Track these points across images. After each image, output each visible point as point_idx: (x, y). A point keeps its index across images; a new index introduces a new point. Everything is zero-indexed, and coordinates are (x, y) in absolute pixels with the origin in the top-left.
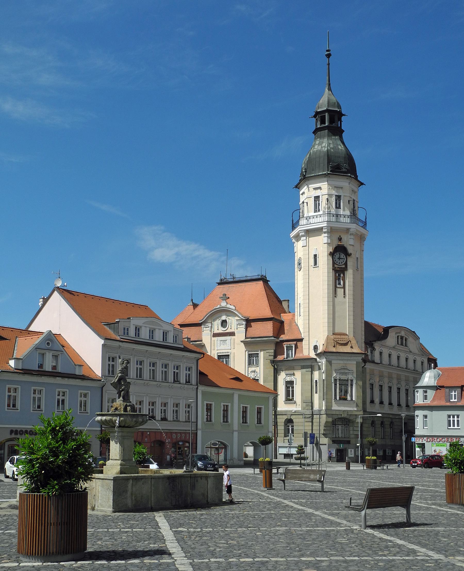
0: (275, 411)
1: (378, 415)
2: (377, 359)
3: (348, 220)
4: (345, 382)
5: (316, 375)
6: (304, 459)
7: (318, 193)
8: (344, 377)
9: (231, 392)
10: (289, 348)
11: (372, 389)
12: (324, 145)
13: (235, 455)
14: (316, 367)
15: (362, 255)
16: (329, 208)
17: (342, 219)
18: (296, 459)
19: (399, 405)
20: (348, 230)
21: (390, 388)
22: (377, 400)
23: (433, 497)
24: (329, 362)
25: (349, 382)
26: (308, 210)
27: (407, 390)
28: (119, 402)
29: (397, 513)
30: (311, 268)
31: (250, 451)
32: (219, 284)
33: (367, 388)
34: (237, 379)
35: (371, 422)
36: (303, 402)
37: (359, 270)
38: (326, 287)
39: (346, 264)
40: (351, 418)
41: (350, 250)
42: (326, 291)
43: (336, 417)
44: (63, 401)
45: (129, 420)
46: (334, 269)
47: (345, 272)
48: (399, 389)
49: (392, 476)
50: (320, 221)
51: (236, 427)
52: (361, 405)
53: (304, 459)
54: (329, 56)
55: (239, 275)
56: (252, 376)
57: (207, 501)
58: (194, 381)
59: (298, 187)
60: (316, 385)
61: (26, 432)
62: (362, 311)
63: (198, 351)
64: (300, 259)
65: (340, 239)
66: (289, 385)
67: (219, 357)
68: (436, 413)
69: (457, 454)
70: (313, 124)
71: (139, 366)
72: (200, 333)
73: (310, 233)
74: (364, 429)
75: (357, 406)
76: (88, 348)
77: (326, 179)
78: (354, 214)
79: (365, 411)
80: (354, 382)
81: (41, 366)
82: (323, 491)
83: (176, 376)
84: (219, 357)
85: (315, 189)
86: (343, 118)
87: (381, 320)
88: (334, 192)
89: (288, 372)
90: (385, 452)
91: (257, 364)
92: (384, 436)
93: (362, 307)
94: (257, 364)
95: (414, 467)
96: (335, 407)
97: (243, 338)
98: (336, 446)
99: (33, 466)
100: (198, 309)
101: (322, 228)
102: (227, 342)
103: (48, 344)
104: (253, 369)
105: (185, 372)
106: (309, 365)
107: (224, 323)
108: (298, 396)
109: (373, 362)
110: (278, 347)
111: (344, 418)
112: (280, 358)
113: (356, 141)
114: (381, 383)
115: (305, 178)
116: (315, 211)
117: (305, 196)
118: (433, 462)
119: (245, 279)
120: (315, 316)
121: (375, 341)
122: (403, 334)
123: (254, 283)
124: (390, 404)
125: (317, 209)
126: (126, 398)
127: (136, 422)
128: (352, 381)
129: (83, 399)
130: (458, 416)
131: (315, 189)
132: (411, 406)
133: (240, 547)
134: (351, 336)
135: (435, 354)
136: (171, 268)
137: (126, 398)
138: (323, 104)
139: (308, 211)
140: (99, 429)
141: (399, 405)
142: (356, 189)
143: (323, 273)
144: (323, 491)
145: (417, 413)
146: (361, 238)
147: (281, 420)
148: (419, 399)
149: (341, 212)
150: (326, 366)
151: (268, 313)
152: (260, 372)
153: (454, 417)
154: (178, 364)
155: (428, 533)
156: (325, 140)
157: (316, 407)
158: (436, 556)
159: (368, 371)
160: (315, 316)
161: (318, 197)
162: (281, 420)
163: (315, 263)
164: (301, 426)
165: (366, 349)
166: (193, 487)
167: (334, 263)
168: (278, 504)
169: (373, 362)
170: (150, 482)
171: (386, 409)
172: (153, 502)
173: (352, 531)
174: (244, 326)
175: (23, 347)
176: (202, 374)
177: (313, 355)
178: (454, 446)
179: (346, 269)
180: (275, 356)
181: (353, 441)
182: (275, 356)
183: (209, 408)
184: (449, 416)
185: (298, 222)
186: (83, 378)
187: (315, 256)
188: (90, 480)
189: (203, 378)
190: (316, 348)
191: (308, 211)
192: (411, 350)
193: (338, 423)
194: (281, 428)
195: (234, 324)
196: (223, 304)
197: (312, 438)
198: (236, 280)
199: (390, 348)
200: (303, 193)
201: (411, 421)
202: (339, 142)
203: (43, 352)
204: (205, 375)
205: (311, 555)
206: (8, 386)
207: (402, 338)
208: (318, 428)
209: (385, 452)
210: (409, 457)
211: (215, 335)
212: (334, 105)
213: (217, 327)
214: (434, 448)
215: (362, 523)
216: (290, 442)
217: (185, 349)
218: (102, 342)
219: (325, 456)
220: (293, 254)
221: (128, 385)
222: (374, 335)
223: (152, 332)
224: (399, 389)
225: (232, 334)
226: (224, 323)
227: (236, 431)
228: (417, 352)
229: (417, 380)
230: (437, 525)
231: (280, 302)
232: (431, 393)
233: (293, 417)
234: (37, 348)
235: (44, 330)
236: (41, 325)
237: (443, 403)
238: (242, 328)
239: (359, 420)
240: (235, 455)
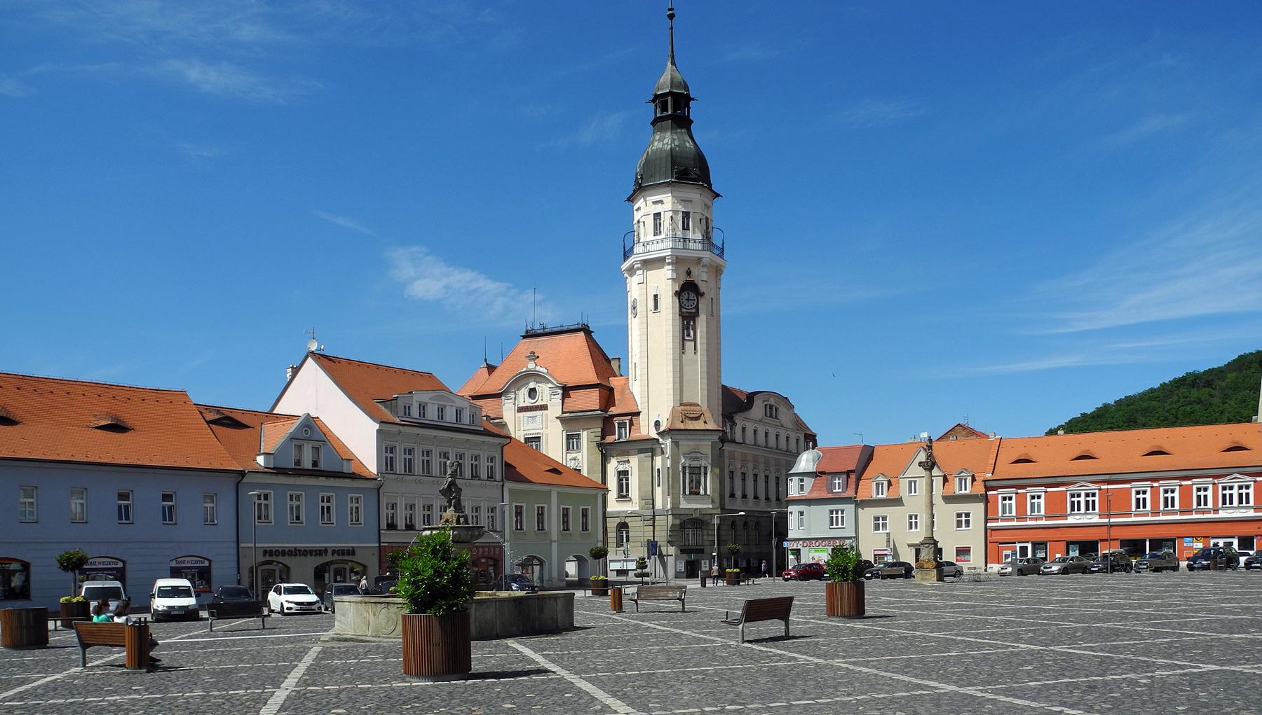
0: (604, 513)
2: (738, 438)
3: (699, 246)
4: (697, 471)
5: (658, 461)
6: (647, 575)
7: (658, 208)
9: (547, 488)
10: (622, 425)
11: (732, 478)
13: (555, 574)
14: (659, 451)
15: (718, 295)
16: (673, 230)
17: (691, 245)
18: (637, 576)
19: (767, 499)
20: (699, 259)
21: (756, 476)
22: (738, 493)
23: (812, 612)
24: (676, 444)
26: (646, 232)
27: (777, 478)
28: (450, 513)
29: (774, 627)
30: (650, 314)
31: (571, 568)
32: (524, 337)
33: (726, 477)
34: (555, 471)
35: (731, 524)
36: (642, 498)
37: (714, 315)
38: (671, 339)
39: (697, 307)
40: (706, 518)
41: (702, 288)
42: (671, 345)
43: (685, 518)
44: (328, 508)
45: (464, 533)
48: (767, 477)
49: (766, 587)
50: (661, 246)
51: (554, 536)
52: (717, 501)
53: (647, 575)
54: (671, 17)
55: (552, 322)
56: (572, 465)
58: (498, 476)
59: (631, 199)
61: (311, 552)
62: (719, 371)
63: (496, 433)
64: (635, 301)
65: (689, 273)
66: (623, 475)
67: (527, 440)
68: (815, 509)
69: (839, 560)
70: (650, 111)
71: (408, 457)
72: (501, 406)
73: (648, 264)
74: (722, 533)
75: (713, 502)
76: (357, 435)
78: (707, 238)
79: (723, 508)
80: (709, 469)
81: (298, 462)
82: (683, 611)
83: (475, 469)
84: (527, 440)
85: (654, 203)
87: (743, 383)
88: (680, 208)
89: (621, 458)
90: (748, 562)
91: (579, 449)
92: (740, 540)
93: (719, 365)
95: (787, 580)
96: (684, 505)
97: (559, 413)
98: (685, 557)
99: (418, 588)
100: (496, 373)
101: (664, 258)
104: (573, 455)
106: (648, 447)
107: (532, 393)
108: (634, 491)
109: (734, 441)
110: (607, 425)
111: (696, 519)
112: (610, 439)
113: (707, 135)
114: (743, 470)
115: (640, 188)
116: (655, 234)
117: (641, 213)
118: (811, 572)
120: (655, 381)
122: (772, 401)
123: (573, 335)
124: (756, 497)
125: (657, 231)
126: (458, 507)
127: (472, 536)
128: (706, 468)
130: (842, 512)
131: (654, 203)
132: (783, 501)
133: (620, 664)
134: (705, 407)
135: (814, 429)
136: (449, 307)
137: (458, 507)
138: (664, 83)
139: (645, 234)
141: (767, 499)
142: (708, 202)
143: (666, 320)
144: (683, 611)
145: (791, 509)
146: (717, 271)
147: (612, 524)
148: (793, 490)
149: (690, 235)
150: (672, 449)
151: (592, 378)
152: (583, 459)
154: (476, 452)
155: (808, 644)
156: (668, 134)
157: (659, 505)
158: (816, 661)
159: (726, 454)
160: (655, 381)
161: (659, 214)
162: (612, 524)
163: (656, 307)
164: (640, 532)
165: (724, 425)
166: (541, 610)
167: (681, 307)
168: (637, 628)
169: (734, 441)
171: (751, 505)
173: (730, 646)
174: (560, 396)
175: (273, 438)
176: (508, 466)
177: (653, 434)
178: (838, 552)
179: (696, 314)
180: (603, 438)
181: (707, 550)
182: (603, 438)
183: (519, 512)
184: (832, 512)
185: (632, 248)
186: (353, 476)
187: (656, 296)
189: (511, 473)
190: (657, 424)
191: (645, 234)
193: (687, 527)
194: (612, 535)
195: (546, 393)
196: (531, 366)
197: (653, 547)
199: (755, 421)
200: (638, 209)
201: (783, 519)
202: (687, 138)
203: (300, 443)
204: (514, 466)
205: (695, 666)
206: (289, 493)
207: (771, 407)
208: (661, 536)
209: (748, 562)
210: (781, 568)
211: (521, 410)
212: (679, 86)
213: (523, 398)
214: (811, 555)
215: (740, 639)
216: (626, 553)
217: (486, 433)
218: (377, 426)
219: (671, 572)
220: (625, 293)
221: (459, 491)
222: (734, 404)
223: (441, 410)
224: (767, 477)
225: (544, 407)
226: (532, 393)
229: (791, 464)
230: (816, 636)
231: (608, 361)
232: (809, 482)
233: (627, 520)
234: (292, 438)
235: (300, 412)
236: (296, 403)
237: (824, 495)
239: (716, 521)
240: (555, 574)
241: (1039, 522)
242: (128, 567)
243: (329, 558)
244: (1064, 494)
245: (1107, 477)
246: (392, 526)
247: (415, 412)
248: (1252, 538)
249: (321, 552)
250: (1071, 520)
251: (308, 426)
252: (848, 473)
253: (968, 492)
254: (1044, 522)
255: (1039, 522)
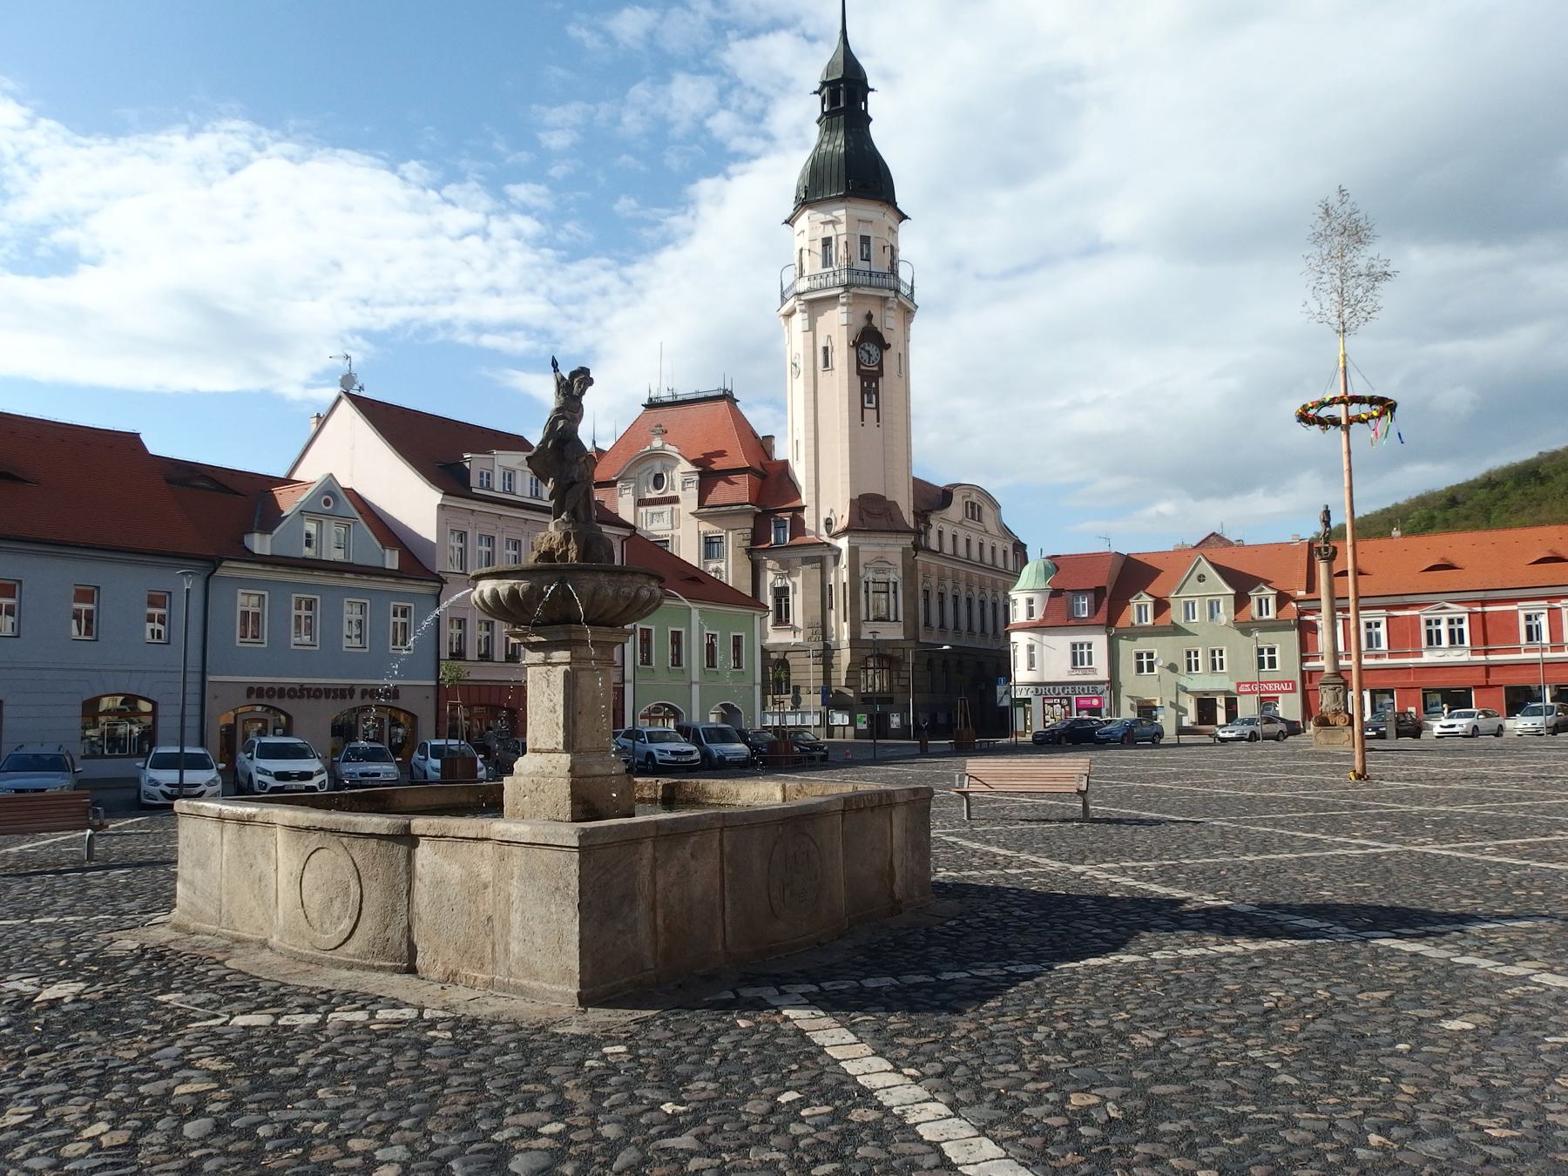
2: (934, 545)
8: (881, 577)
15: (906, 348)
39: (880, 365)
46: (859, 372)
51: (696, 676)
57: (892, 895)
65: (869, 317)
86: (870, 95)
94: (720, 557)
101: (837, 296)
103: (327, 503)
108: (797, 616)
109: (928, 550)
116: (825, 266)
122: (974, 498)
130: (1090, 646)
140: (433, 683)
153: (1082, 646)
170: (716, 844)
172: (729, 929)
181: (898, 698)
190: (828, 523)
207: (973, 504)
225: (675, 500)
228: (996, 532)
238: (693, 491)
241: (1379, 661)
242: (161, 711)
243: (357, 701)
244: (1416, 619)
245: (1480, 595)
247: (498, 484)
248: (1469, 691)
249: (345, 693)
250: (1429, 657)
251: (329, 493)
252: (1098, 593)
253: (1272, 615)
254: (1386, 661)
255: (1379, 661)
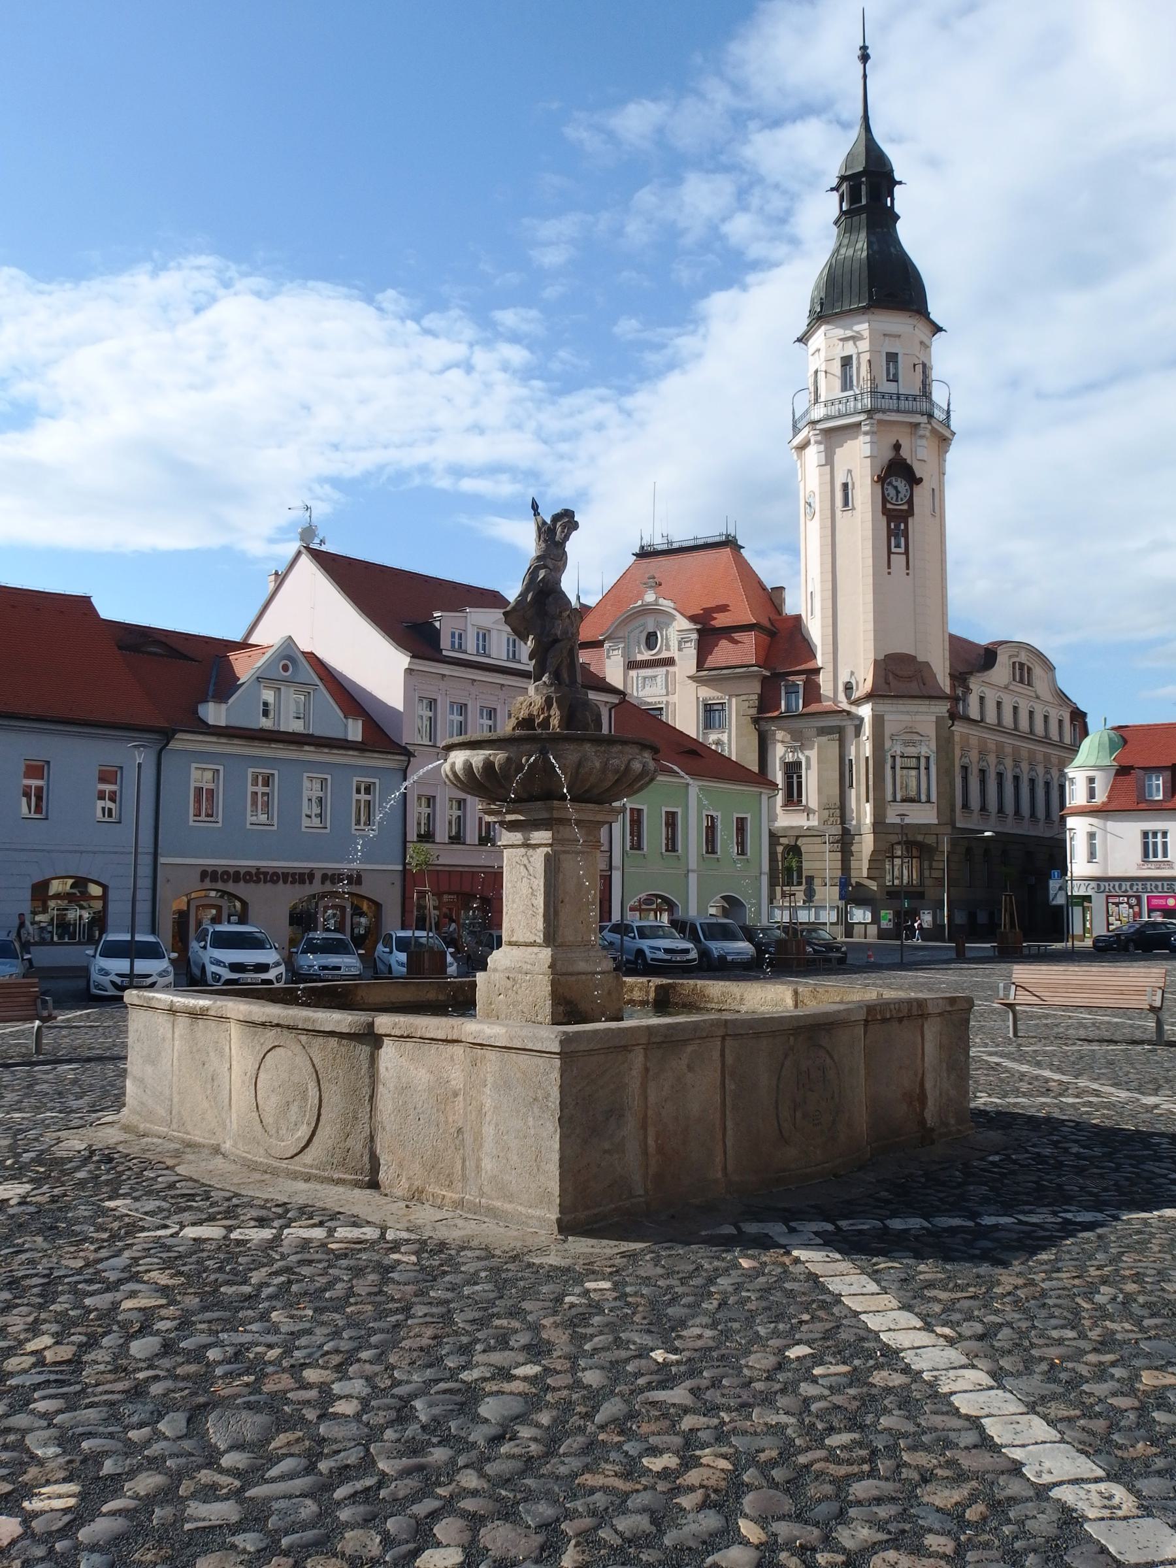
1: (987, 834)
2: (974, 713)
7: (849, 349)
12: (859, 245)
25: (923, 761)
30: (838, 513)
39: (910, 502)
46: (885, 511)
47: (910, 520)
51: (693, 865)
60: (851, 771)
65: (897, 447)
77: (865, 317)
86: (897, 189)
94: (722, 727)
97: (692, 670)
102: (659, 679)
103: (285, 668)
105: (448, 812)
109: (967, 719)
119: (691, 543)
121: (971, 673)
122: (1023, 657)
129: (363, 797)
130: (1165, 834)
140: (400, 868)
153: (1155, 834)
159: (957, 738)
167: (885, 500)
181: (930, 893)
188: (630, 1051)
190: (848, 688)
192: (1040, 693)
198: (675, 546)
207: (1022, 665)
225: (670, 662)
227: (693, 871)
238: (691, 651)
243: (316, 887)
246: (427, 837)
247: (471, 645)
